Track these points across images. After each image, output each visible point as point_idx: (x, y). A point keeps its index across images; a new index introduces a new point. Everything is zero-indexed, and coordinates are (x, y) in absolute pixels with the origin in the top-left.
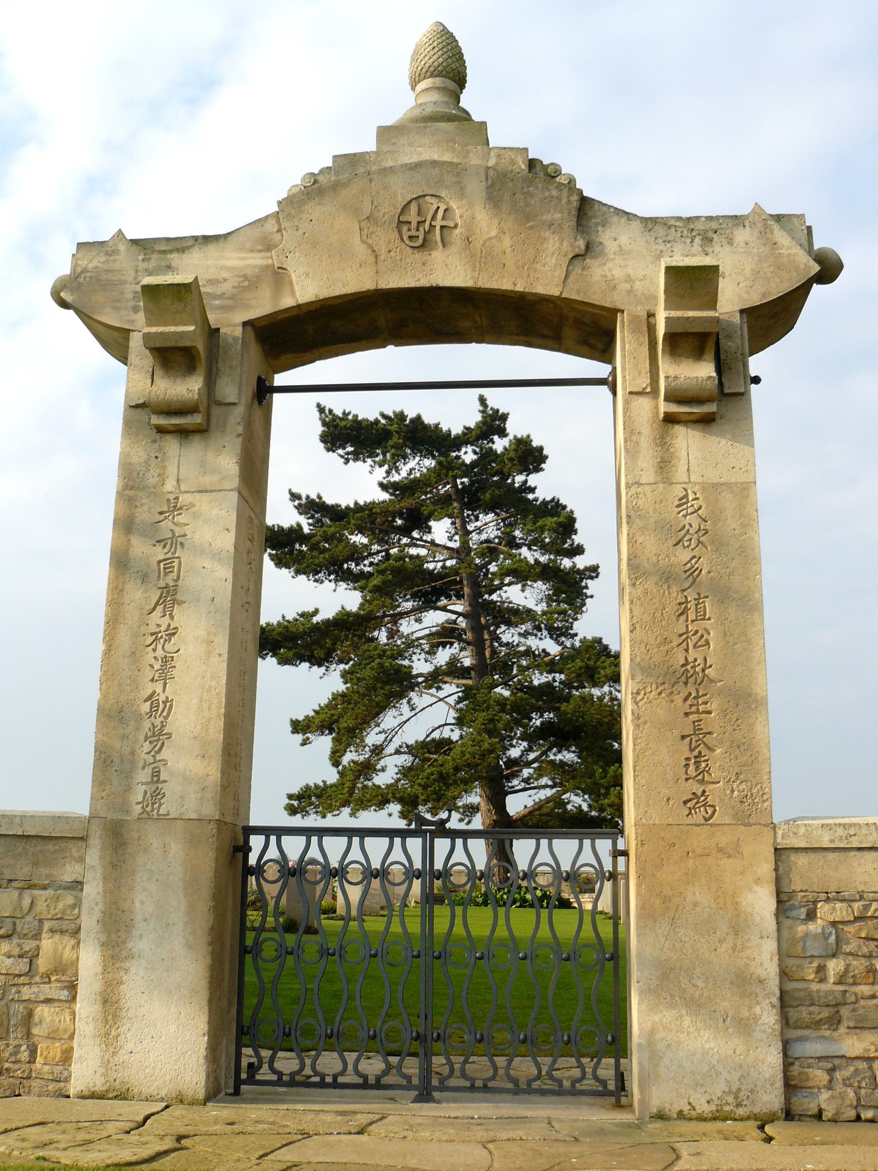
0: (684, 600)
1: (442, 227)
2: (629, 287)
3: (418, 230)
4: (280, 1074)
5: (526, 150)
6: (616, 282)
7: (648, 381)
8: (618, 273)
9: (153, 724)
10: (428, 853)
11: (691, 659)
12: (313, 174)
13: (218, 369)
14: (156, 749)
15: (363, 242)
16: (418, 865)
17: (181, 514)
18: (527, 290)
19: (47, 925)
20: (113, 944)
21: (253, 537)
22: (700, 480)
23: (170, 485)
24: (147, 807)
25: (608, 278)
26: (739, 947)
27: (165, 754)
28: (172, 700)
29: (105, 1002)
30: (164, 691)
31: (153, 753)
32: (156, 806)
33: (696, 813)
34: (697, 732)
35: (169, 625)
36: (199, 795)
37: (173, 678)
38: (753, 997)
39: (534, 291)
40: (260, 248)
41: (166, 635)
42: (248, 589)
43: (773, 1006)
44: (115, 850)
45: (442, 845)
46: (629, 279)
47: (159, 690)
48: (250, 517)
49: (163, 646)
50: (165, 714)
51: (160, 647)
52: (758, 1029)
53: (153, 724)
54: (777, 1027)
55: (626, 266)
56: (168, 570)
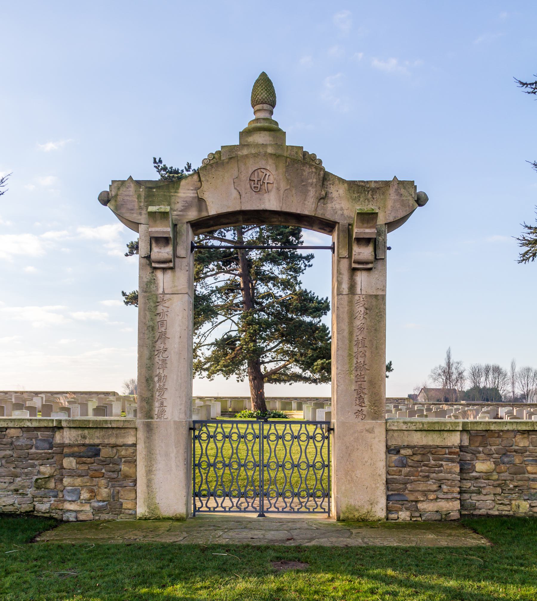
1: (267, 183)
3: (258, 184)
4: (209, 508)
5: (302, 148)
8: (338, 206)
10: (262, 429)
11: (359, 362)
12: (212, 154)
15: (235, 189)
16: (265, 440)
19: (123, 460)
23: (161, 291)
27: (165, 396)
29: (148, 486)
40: (192, 188)
43: (383, 484)
44: (148, 432)
46: (342, 209)
47: (161, 372)
54: (385, 491)
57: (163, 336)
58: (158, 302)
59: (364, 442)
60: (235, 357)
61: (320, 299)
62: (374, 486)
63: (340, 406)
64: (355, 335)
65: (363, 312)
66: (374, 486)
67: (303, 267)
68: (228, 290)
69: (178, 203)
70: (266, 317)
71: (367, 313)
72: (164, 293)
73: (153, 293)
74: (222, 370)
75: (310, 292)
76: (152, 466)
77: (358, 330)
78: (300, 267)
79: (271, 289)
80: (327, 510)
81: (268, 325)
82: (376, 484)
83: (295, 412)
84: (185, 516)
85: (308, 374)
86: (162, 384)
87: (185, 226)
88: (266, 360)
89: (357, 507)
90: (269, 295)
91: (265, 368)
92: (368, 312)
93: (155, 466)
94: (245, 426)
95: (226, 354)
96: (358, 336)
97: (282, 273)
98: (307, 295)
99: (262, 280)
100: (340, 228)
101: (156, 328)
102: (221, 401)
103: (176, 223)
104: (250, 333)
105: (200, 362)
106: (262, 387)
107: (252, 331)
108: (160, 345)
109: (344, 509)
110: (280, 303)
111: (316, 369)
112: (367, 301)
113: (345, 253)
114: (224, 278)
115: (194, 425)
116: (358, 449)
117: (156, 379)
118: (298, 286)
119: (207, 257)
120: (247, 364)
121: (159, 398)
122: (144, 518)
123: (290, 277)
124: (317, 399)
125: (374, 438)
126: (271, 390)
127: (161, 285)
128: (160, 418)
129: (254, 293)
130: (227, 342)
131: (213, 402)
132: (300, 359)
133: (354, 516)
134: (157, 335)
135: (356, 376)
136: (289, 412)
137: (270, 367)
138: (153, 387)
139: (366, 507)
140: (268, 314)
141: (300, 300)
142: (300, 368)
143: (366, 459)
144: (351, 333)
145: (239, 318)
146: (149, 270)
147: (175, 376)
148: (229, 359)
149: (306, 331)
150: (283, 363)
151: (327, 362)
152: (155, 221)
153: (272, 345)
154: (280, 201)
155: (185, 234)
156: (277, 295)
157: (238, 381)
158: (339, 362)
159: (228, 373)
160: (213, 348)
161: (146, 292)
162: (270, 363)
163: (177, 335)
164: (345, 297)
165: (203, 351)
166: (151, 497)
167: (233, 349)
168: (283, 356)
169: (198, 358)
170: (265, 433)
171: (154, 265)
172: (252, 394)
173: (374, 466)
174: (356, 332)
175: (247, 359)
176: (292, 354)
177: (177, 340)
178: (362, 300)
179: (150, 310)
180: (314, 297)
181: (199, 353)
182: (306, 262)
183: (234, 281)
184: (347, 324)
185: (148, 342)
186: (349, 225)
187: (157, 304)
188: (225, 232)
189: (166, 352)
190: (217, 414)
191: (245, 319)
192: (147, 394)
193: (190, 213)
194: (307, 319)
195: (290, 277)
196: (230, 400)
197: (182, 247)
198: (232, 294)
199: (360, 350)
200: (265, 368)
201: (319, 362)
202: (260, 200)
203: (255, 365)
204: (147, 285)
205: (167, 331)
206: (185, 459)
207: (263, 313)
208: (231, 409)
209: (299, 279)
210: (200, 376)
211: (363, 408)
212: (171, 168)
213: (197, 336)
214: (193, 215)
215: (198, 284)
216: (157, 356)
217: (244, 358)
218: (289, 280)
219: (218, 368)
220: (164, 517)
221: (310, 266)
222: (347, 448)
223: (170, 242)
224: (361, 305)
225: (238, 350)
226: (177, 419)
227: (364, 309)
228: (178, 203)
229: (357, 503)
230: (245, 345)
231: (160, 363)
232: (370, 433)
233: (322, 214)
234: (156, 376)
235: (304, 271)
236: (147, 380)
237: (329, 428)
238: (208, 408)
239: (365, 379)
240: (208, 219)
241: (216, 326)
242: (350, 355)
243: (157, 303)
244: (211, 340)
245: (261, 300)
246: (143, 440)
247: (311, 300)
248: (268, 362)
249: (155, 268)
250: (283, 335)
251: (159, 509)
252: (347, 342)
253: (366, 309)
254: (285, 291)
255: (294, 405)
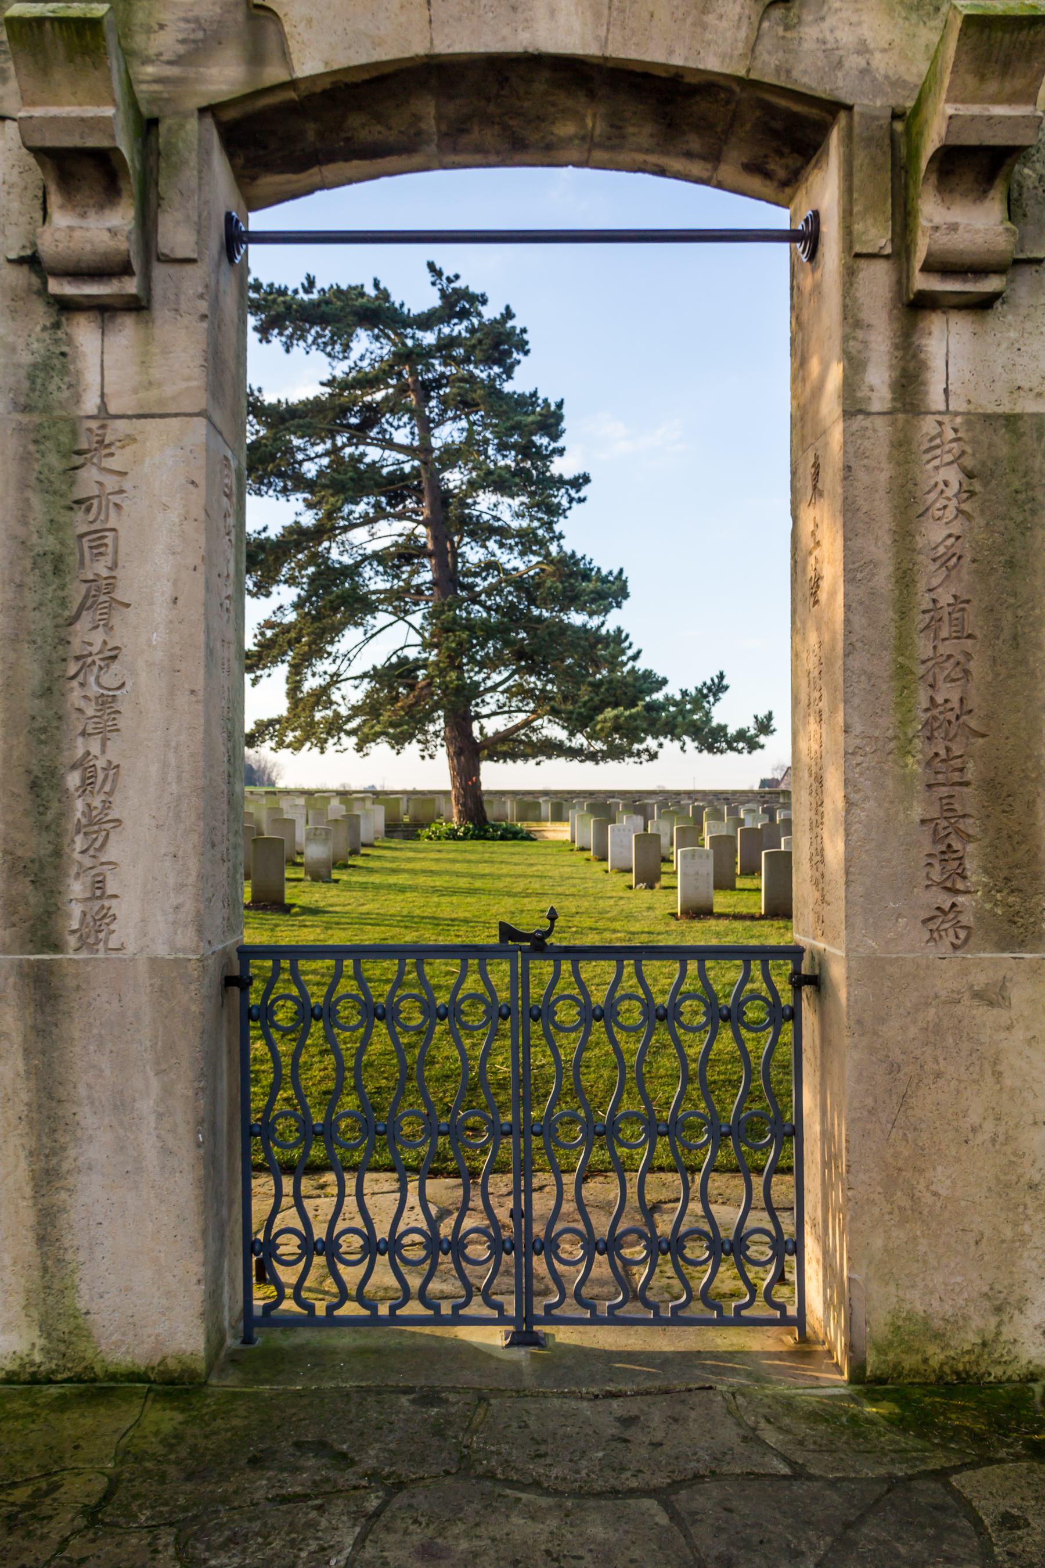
0: (931, 606)
2: (863, 63)
6: (841, 52)
7: (890, 236)
8: (846, 37)
9: (89, 805)
10: (520, 980)
11: (940, 700)
13: (159, 197)
14: (97, 845)
17: (112, 455)
18: (691, 64)
20: (47, 1151)
21: (231, 489)
22: (963, 407)
23: (90, 404)
24: (88, 937)
25: (829, 46)
26: (1002, 1138)
27: (112, 853)
28: (118, 766)
29: (41, 1240)
30: (103, 752)
31: (91, 852)
32: (101, 936)
33: (941, 936)
34: (946, 814)
35: (105, 643)
36: (171, 918)
37: (118, 730)
38: (1021, 1209)
39: (701, 67)
41: (102, 659)
42: (228, 576)
45: (542, 969)
46: (863, 48)
47: (95, 748)
48: (226, 458)
49: (98, 678)
50: (107, 789)
51: (92, 679)
52: (1026, 1254)
53: (89, 805)
55: (860, 24)
56: (98, 549)
57: (103, 599)
58: (79, 453)
59: (966, 1046)
60: (416, 703)
61: (604, 572)
62: (1008, 1233)
63: (860, 890)
64: (922, 586)
65: (955, 487)
66: (1008, 1233)
67: (565, 503)
68: (400, 556)
69: (162, 27)
70: (485, 615)
71: (972, 494)
72: (104, 414)
73: (58, 412)
74: (387, 734)
75: (583, 558)
76: (57, 1151)
77: (933, 567)
78: (559, 503)
79: (494, 555)
80: (792, 1311)
81: (488, 631)
82: (1016, 1224)
83: (549, 824)
84: (201, 1366)
85: (580, 740)
86: (97, 802)
87: (192, 125)
88: (485, 710)
89: (937, 1324)
90: (491, 566)
91: (482, 728)
92: (977, 486)
93: (72, 1153)
94: (454, 965)
95: (396, 699)
96: (938, 589)
97: (518, 515)
98: (577, 563)
99: (472, 534)
100: (857, 130)
101: (72, 560)
102: (386, 803)
103: (156, 112)
104: (448, 649)
105: (337, 715)
106: (477, 772)
107: (453, 645)
108: (86, 635)
109: (879, 1325)
110: (516, 582)
111: (602, 729)
112: (974, 441)
113: (877, 236)
114: (388, 533)
115: (245, 966)
116: (938, 1075)
117: (73, 780)
118: (555, 543)
119: (352, 479)
120: (442, 720)
121: (87, 862)
122: (24, 1377)
123: (536, 524)
124: (591, 793)
125: (1009, 1028)
126: (496, 776)
127: (91, 377)
128: (92, 948)
129: (456, 563)
130: (396, 674)
131: (368, 804)
132: (563, 707)
133: (925, 1361)
134: (77, 592)
135: (928, 764)
136: (534, 824)
137: (494, 725)
138: (62, 815)
139: (976, 1322)
140: (488, 609)
141: (560, 576)
142: (563, 727)
143: (974, 1118)
144: (905, 579)
145: (424, 617)
146: (41, 314)
147: (154, 770)
148: (402, 708)
149: (573, 645)
150: (521, 717)
151: (627, 713)
152: (44, 70)
153: (496, 678)
154: (597, 15)
155: (193, 159)
156: (508, 566)
157: (423, 757)
158: (856, 701)
159: (399, 741)
160: (366, 685)
161: (27, 409)
162: (493, 718)
163: (163, 591)
164: (880, 423)
165: (343, 692)
166: (57, 1285)
167: (411, 687)
168: (521, 701)
169: (335, 707)
170: (536, 992)
171: (55, 287)
172: (454, 786)
173: (1008, 1149)
174: (929, 575)
175: (442, 708)
176: (542, 698)
177: (161, 611)
178: (950, 435)
179: (45, 486)
180: (591, 570)
181: (336, 696)
182: (572, 492)
183: (411, 537)
184: (887, 539)
185: (42, 621)
186: (896, 116)
187: (77, 460)
188: (392, 430)
189: (115, 667)
190: (376, 832)
191: (438, 618)
192: (35, 846)
193: (214, 71)
194: (576, 618)
195: (536, 524)
196: (405, 797)
197: (179, 216)
198: (408, 568)
199: (944, 649)
200: (482, 728)
201: (610, 713)
202: (514, 9)
203: (460, 722)
204: (32, 378)
205: (119, 573)
206: (201, 1123)
207: (477, 607)
208: (407, 819)
209: (557, 528)
210: (338, 747)
211: (961, 899)
212: (271, 285)
213: (331, 659)
214: (224, 77)
215: (334, 545)
216: (75, 683)
217: (435, 707)
218: (536, 528)
219: (378, 728)
220: (112, 1369)
221: (581, 500)
222: (894, 1069)
223: (122, 185)
224: (948, 458)
225: (422, 689)
226: (162, 951)
227: (961, 476)
228: (162, 27)
229: (936, 1303)
230: (439, 676)
231: (90, 712)
232: (991, 1004)
233: (778, 69)
234: (73, 767)
235: (568, 513)
236: (34, 786)
237: (796, 972)
238: (352, 822)
239: (969, 776)
240: (291, 109)
241: (373, 636)
242: (902, 672)
243: (76, 458)
244: (363, 664)
245: (471, 580)
246: (17, 1039)
247: (586, 576)
248: (488, 716)
249: (66, 306)
250: (520, 655)
251: (89, 1336)
252: (888, 615)
253: (970, 475)
254: (526, 559)
255: (546, 809)
